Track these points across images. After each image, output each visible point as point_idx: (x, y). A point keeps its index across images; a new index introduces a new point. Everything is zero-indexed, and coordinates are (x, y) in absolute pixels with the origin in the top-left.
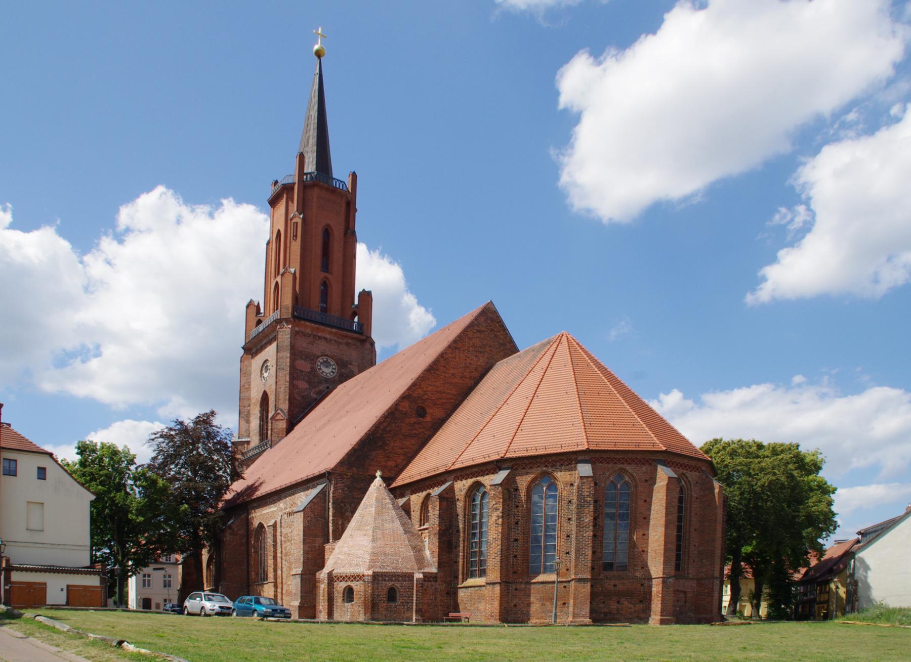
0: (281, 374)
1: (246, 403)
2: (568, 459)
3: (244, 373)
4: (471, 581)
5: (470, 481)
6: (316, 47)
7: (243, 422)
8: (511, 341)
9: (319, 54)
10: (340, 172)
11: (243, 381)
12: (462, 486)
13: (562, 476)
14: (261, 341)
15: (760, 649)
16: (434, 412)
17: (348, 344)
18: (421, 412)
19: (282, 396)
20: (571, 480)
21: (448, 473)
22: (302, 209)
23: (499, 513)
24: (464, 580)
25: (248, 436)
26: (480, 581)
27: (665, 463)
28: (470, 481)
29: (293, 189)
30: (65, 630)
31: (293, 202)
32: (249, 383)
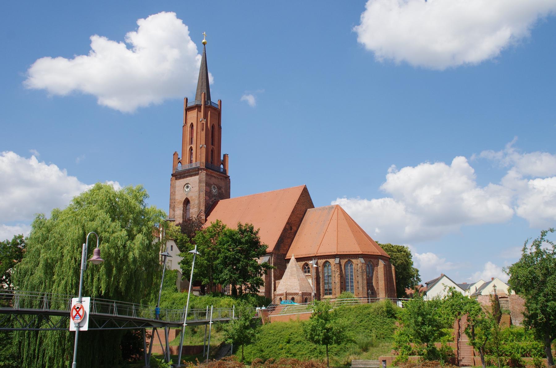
0: (201, 193)
1: (173, 201)
2: (356, 256)
3: (173, 187)
4: (326, 297)
5: (324, 260)
6: (204, 41)
7: (171, 210)
8: (312, 203)
9: (204, 44)
10: (214, 99)
12: (321, 262)
13: (354, 261)
14: (185, 173)
16: (294, 228)
17: (221, 179)
18: (291, 229)
19: (202, 204)
21: (316, 256)
23: (339, 273)
24: (323, 296)
26: (331, 296)
27: (382, 259)
28: (324, 260)
30: (417, 357)
31: (200, 112)
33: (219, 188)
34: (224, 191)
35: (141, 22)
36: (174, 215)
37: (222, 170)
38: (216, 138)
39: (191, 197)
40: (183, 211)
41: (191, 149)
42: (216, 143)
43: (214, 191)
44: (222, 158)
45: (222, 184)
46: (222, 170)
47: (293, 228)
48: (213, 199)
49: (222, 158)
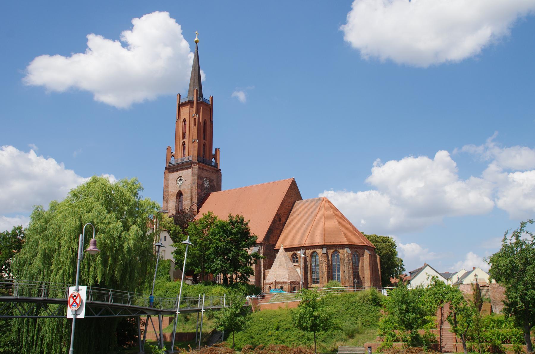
0: (194, 186)
1: (167, 194)
2: (343, 246)
4: (313, 285)
5: (312, 251)
6: (196, 39)
7: (165, 202)
8: (300, 196)
9: (196, 42)
10: (206, 95)
11: (166, 183)
12: (309, 252)
14: (178, 167)
15: (33, 309)
16: (283, 220)
17: (213, 172)
18: (280, 220)
19: (194, 196)
20: (345, 253)
21: (304, 247)
22: (198, 112)
23: (326, 263)
24: (311, 285)
25: (168, 209)
27: (367, 249)
28: (312, 251)
29: (193, 103)
31: (193, 107)
32: (168, 185)
33: (211, 181)
34: (215, 183)
35: (136, 22)
36: (167, 206)
37: (213, 164)
38: (208, 133)
39: (184, 189)
40: (176, 203)
41: (184, 143)
42: (208, 138)
43: (206, 183)
44: (213, 152)
45: (214, 177)
46: (213, 164)
47: (282, 219)
48: (205, 191)
49: (213, 152)
